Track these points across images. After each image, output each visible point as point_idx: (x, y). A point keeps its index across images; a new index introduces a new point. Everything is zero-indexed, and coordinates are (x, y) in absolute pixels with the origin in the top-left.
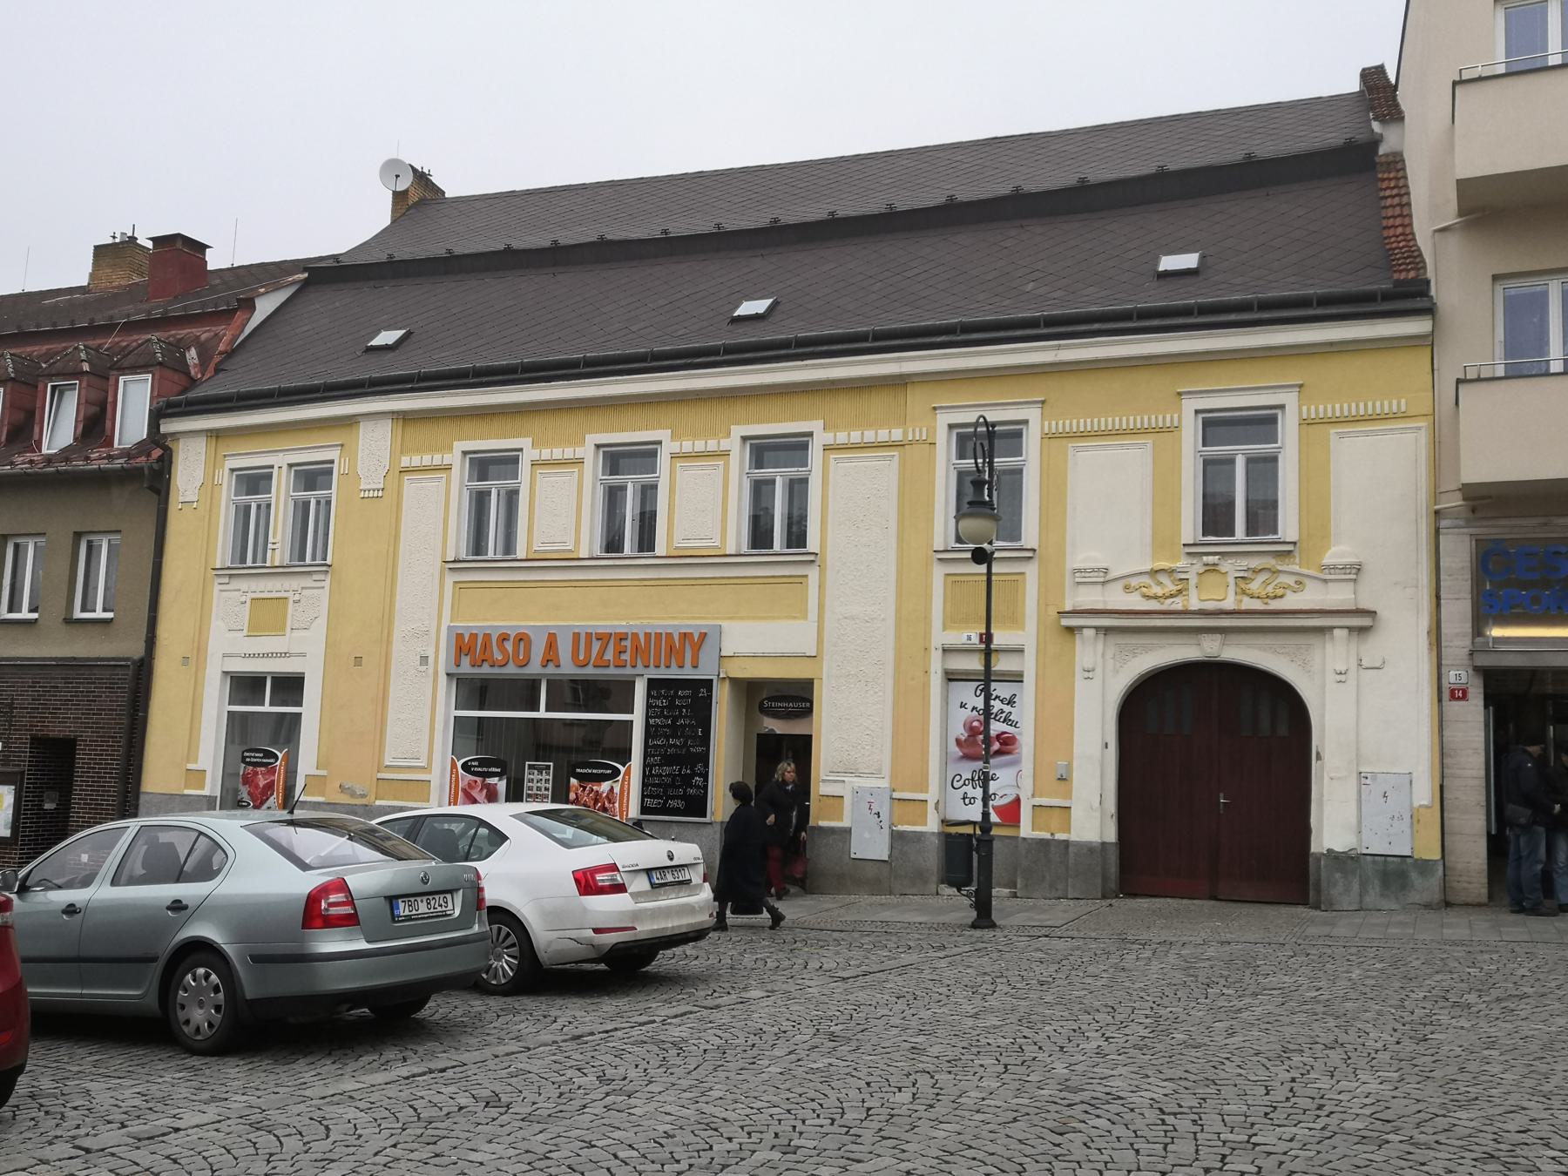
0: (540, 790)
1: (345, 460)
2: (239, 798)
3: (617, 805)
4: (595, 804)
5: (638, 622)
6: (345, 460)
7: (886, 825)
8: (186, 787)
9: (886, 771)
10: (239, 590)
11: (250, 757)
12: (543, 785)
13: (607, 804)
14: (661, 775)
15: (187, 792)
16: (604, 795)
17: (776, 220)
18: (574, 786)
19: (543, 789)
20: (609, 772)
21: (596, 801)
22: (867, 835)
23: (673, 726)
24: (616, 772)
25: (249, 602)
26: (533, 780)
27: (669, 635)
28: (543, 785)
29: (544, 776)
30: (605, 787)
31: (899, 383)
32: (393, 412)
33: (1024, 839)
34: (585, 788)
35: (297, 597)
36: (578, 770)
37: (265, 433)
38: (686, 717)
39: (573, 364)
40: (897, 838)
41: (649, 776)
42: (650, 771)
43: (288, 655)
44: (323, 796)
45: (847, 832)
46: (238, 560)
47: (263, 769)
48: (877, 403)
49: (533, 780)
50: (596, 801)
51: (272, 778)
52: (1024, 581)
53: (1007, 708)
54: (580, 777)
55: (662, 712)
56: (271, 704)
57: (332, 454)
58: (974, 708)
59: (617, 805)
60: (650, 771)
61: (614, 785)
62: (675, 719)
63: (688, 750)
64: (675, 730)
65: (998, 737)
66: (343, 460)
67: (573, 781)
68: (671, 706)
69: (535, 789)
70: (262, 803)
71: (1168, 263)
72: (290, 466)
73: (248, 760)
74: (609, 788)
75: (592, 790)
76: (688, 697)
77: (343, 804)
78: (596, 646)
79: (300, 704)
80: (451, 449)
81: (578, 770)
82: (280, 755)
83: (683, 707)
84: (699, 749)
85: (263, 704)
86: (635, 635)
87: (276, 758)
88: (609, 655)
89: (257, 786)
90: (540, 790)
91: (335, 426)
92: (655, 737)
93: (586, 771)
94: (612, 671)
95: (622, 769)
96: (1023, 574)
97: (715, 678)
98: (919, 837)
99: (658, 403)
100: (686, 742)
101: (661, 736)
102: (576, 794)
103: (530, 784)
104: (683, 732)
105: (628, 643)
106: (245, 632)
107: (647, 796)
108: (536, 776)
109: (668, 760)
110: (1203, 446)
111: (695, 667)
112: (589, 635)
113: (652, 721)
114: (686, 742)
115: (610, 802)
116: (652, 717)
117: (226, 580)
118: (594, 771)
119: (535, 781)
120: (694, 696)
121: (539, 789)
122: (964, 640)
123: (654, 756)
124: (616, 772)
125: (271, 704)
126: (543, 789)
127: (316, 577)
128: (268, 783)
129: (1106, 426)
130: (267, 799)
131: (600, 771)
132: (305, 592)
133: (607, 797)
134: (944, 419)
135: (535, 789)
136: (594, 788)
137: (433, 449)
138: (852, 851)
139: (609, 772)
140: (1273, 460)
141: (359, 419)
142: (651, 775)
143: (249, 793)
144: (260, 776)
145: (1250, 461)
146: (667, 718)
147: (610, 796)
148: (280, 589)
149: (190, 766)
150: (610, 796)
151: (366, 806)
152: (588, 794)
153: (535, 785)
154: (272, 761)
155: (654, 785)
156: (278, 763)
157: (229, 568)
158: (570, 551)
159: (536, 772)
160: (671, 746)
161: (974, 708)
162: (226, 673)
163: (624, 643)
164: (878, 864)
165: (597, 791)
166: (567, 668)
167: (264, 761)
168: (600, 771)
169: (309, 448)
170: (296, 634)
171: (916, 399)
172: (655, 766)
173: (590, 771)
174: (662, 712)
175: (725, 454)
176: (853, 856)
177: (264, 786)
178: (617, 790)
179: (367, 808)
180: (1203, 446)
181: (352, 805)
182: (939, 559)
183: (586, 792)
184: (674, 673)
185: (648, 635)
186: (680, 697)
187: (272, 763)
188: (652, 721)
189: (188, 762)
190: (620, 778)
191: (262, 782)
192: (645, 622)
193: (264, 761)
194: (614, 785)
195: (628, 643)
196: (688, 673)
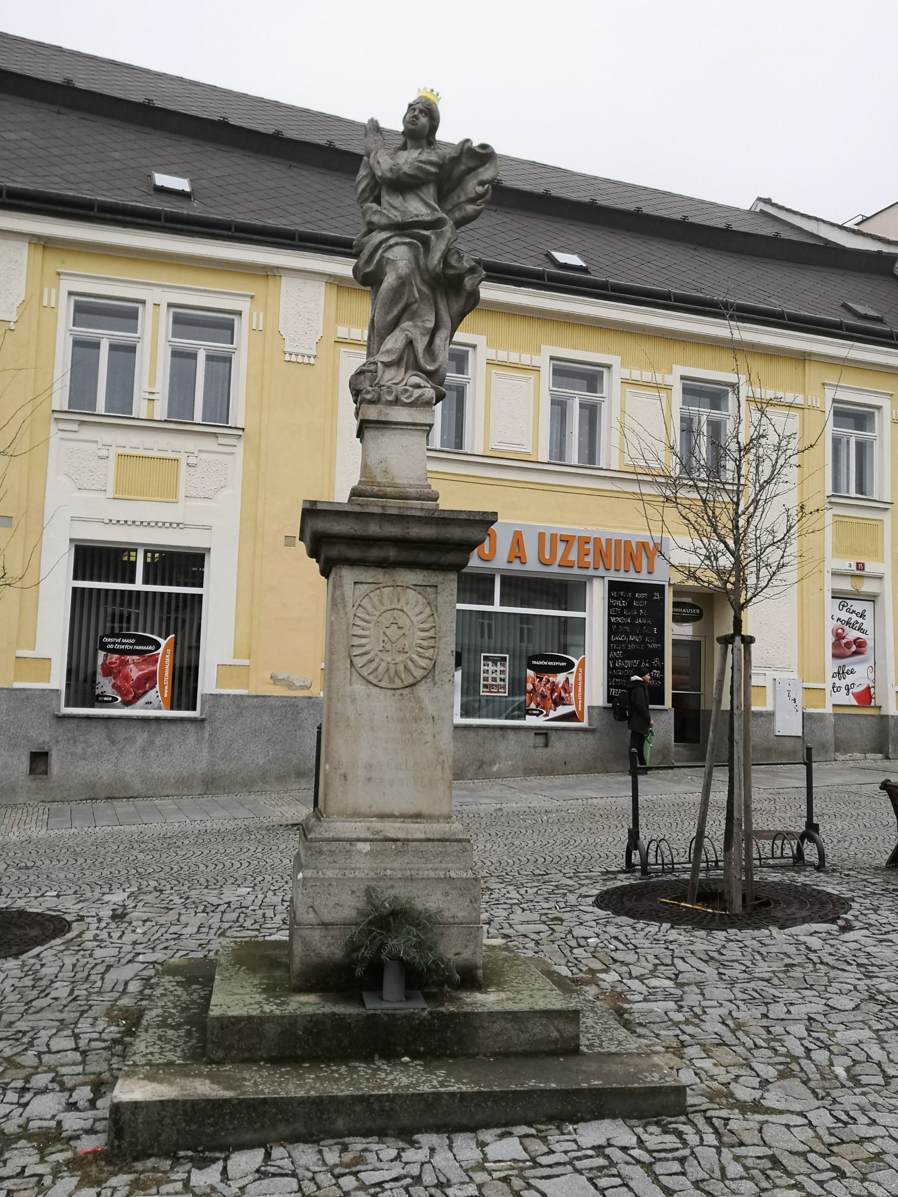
0: (496, 681)
1: (50, 292)
2: (98, 692)
3: (572, 694)
4: (552, 694)
5: (594, 528)
6: (50, 292)
7: (800, 708)
8: (17, 678)
9: (795, 668)
10: (96, 442)
11: (114, 643)
12: (498, 676)
13: (563, 694)
14: (623, 668)
15: (17, 685)
16: (560, 686)
17: (69, 81)
18: (530, 677)
19: (498, 680)
20: (563, 664)
21: (553, 691)
22: (787, 717)
23: (632, 625)
24: (571, 665)
25: (113, 459)
26: (488, 671)
27: (628, 543)
28: (490, 676)
29: (499, 668)
30: (560, 678)
31: (803, 358)
32: (34, 236)
33: (892, 716)
34: (541, 679)
35: (192, 460)
36: (534, 662)
37: (215, 271)
38: (643, 616)
39: (666, 296)
40: (807, 718)
41: (613, 669)
42: (614, 664)
43: (181, 526)
44: (248, 688)
45: (771, 715)
46: (586, 460)
47: (136, 657)
48: (785, 370)
49: (488, 671)
50: (553, 691)
51: (152, 668)
52: (883, 525)
53: (860, 620)
54: (539, 670)
55: (622, 611)
56: (502, 604)
57: (242, 305)
58: (839, 619)
59: (572, 694)
60: (614, 664)
61: (569, 676)
62: (634, 618)
63: (646, 647)
64: (634, 628)
65: (855, 641)
66: (255, 314)
67: (530, 673)
68: (630, 607)
69: (490, 679)
70: (137, 698)
71: (162, 180)
72: (170, 305)
73: (110, 646)
74: (564, 679)
75: (549, 681)
76: (644, 599)
77: (277, 697)
78: (561, 547)
79: (201, 586)
80: (538, 351)
81: (534, 662)
82: (163, 642)
83: (640, 608)
84: (655, 646)
85: (132, 581)
86: (597, 540)
87: (158, 645)
88: (573, 556)
89: (127, 678)
90: (496, 681)
91: (100, 255)
92: (616, 634)
93: (541, 663)
94: (575, 571)
95: (576, 662)
96: (881, 520)
97: (666, 584)
98: (821, 717)
99: (772, 356)
100: (644, 639)
101: (621, 633)
102: (533, 685)
103: (486, 675)
104: (641, 629)
105: (590, 546)
106: (110, 493)
107: (612, 687)
108: (491, 668)
109: (628, 655)
110: (74, 325)
111: (650, 573)
112: (554, 536)
113: (613, 619)
114: (644, 639)
115: (566, 692)
116: (613, 616)
117: (75, 427)
118: (550, 663)
119: (490, 672)
120: (649, 598)
121: (494, 679)
122: (847, 567)
123: (616, 650)
124: (571, 665)
125: (502, 604)
126: (498, 680)
127: (222, 440)
128: (144, 675)
129: (49, 301)
130: (145, 692)
131: (556, 664)
132: (203, 456)
133: (563, 687)
134: (830, 394)
135: (490, 679)
136: (551, 679)
137: (654, 368)
138: (777, 729)
139: (563, 664)
140: (132, 349)
141: (282, 272)
142: (616, 668)
143: (114, 686)
144: (132, 666)
145: (113, 348)
146: (625, 616)
147: (566, 687)
148: (165, 448)
149: (21, 653)
150: (566, 687)
151: (310, 698)
152: (545, 685)
153: (490, 676)
154: (150, 648)
155: (618, 677)
156: (161, 651)
157: (166, 421)
158: (528, 454)
159: (490, 663)
160: (631, 642)
161: (839, 619)
162: (71, 540)
163: (587, 546)
164: (794, 739)
165: (553, 682)
166: (532, 566)
167: (137, 648)
168: (556, 664)
169: (877, 393)
170: (192, 503)
171: (814, 374)
172: (618, 659)
173: (545, 663)
174: (622, 611)
175: (536, 370)
176: (778, 734)
177: (139, 678)
178: (572, 681)
179: (312, 700)
180: (74, 325)
181: (292, 698)
182: (56, 419)
183: (543, 683)
184: (631, 577)
185: (609, 541)
186: (637, 599)
187: (151, 651)
188: (613, 619)
189: (19, 646)
190: (574, 670)
191: (135, 673)
192: (601, 529)
193: (137, 648)
194: (569, 676)
195: (590, 546)
196: (643, 578)
